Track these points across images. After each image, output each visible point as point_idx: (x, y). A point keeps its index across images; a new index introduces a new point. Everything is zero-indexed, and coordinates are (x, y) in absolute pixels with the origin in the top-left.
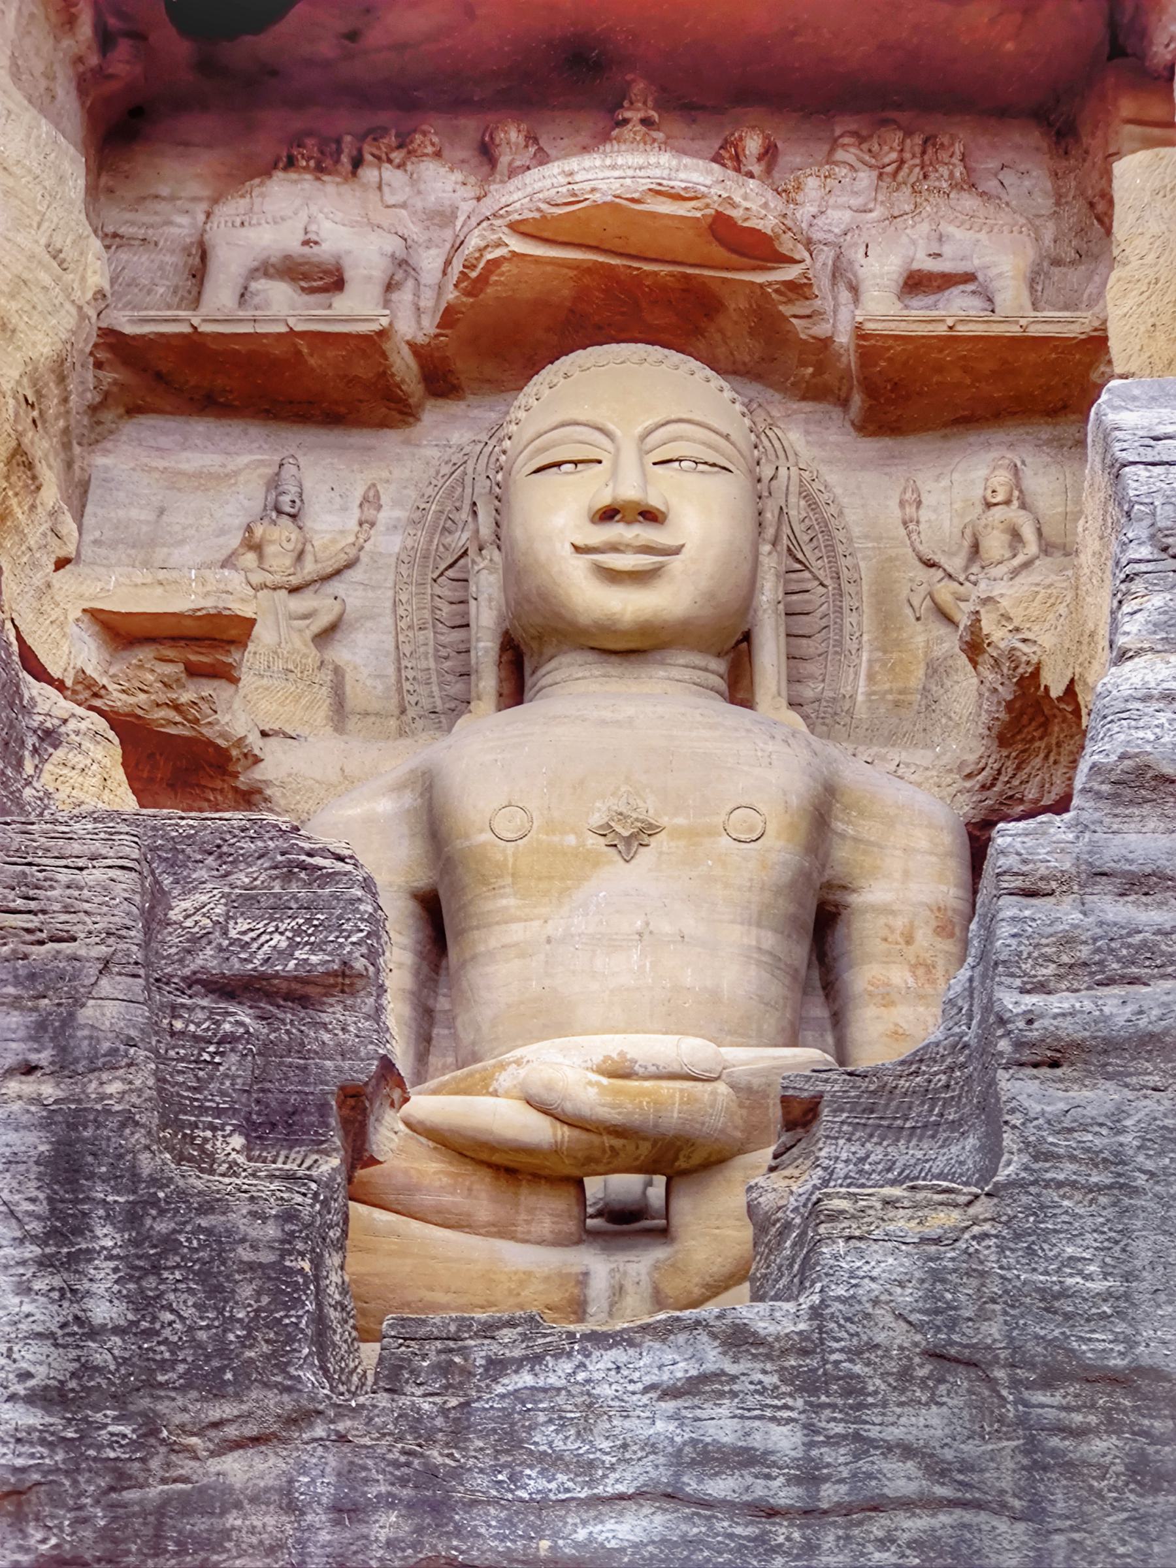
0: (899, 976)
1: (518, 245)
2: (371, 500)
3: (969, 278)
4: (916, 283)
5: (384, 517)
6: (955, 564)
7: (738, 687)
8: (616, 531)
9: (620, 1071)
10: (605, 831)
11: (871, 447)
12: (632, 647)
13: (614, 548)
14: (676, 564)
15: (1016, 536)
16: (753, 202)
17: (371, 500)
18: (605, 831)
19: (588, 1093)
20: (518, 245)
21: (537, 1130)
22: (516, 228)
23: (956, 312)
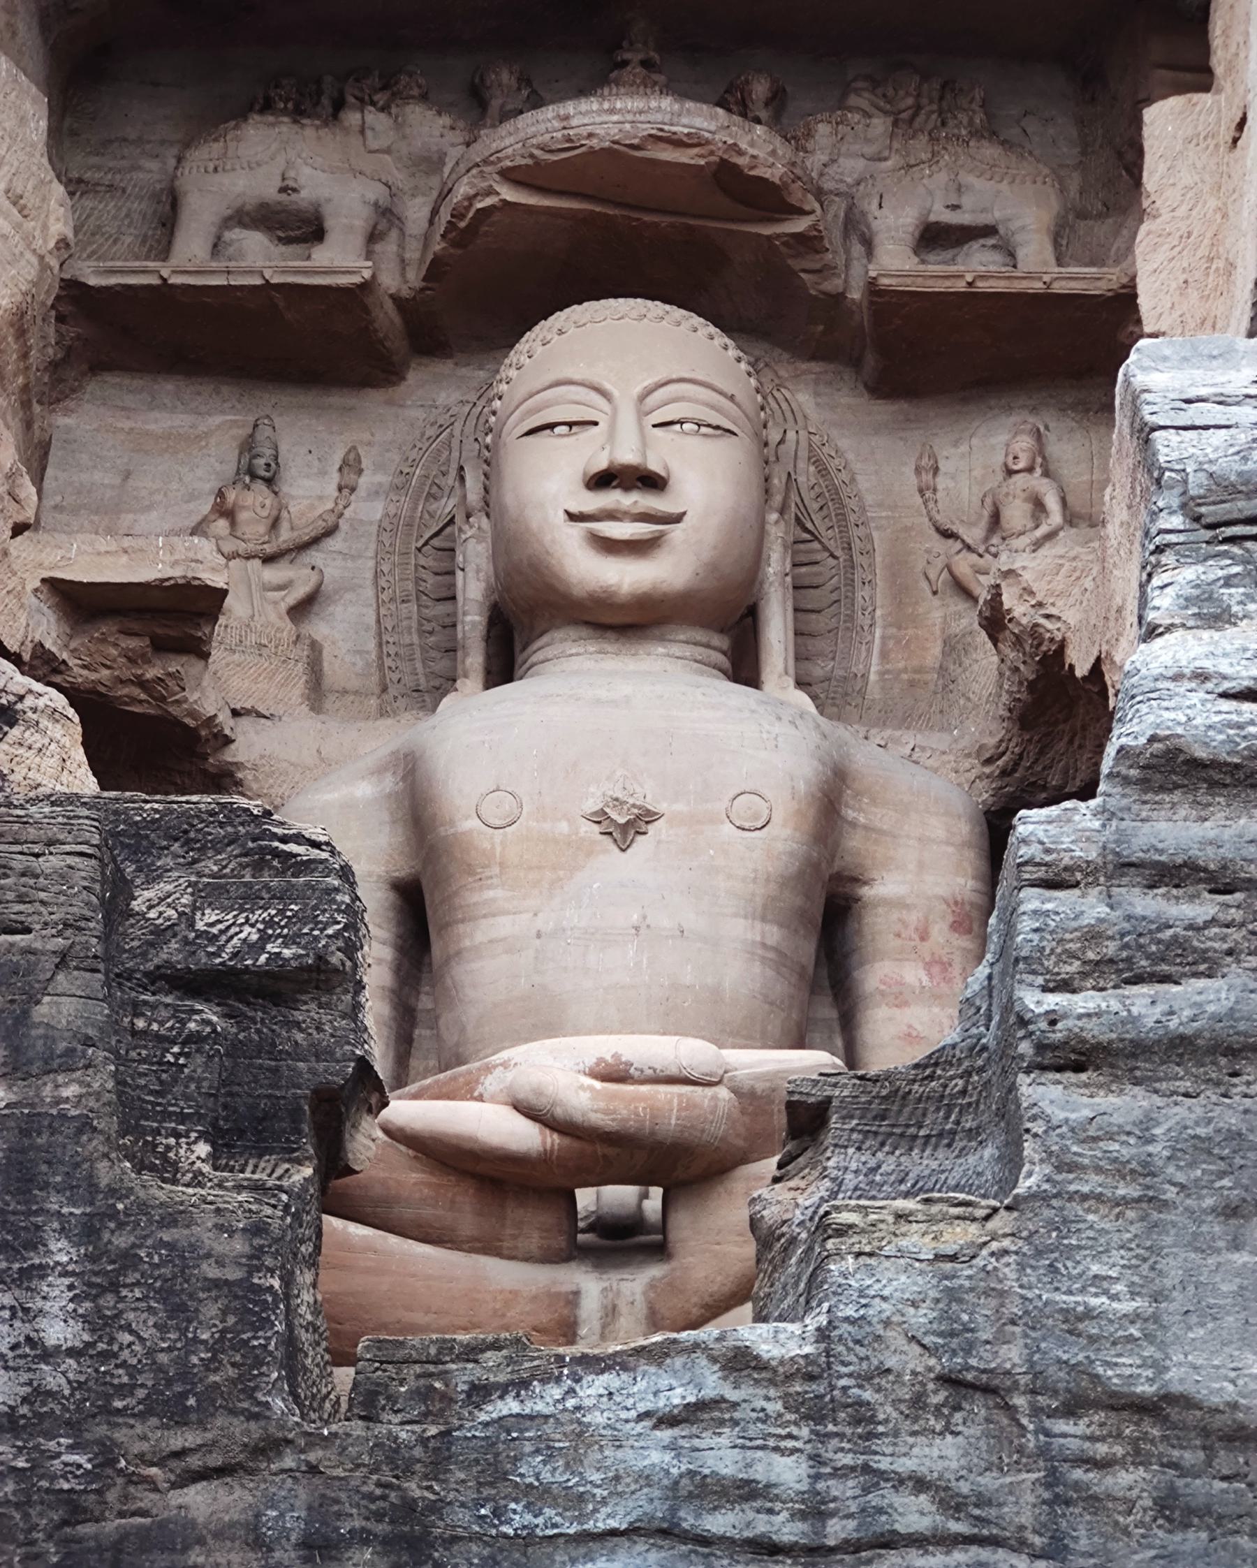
0: (914, 974)
1: (509, 194)
2: (351, 465)
3: (989, 231)
4: (934, 238)
5: (365, 481)
6: (974, 535)
7: (743, 667)
8: (614, 498)
9: (615, 1074)
10: (599, 818)
11: (884, 410)
12: (627, 622)
13: (611, 515)
14: (676, 533)
15: (1039, 506)
16: (760, 148)
17: (351, 465)
18: (599, 818)
19: (582, 1098)
20: (509, 194)
21: (523, 1136)
22: (511, 176)
23: (975, 268)
